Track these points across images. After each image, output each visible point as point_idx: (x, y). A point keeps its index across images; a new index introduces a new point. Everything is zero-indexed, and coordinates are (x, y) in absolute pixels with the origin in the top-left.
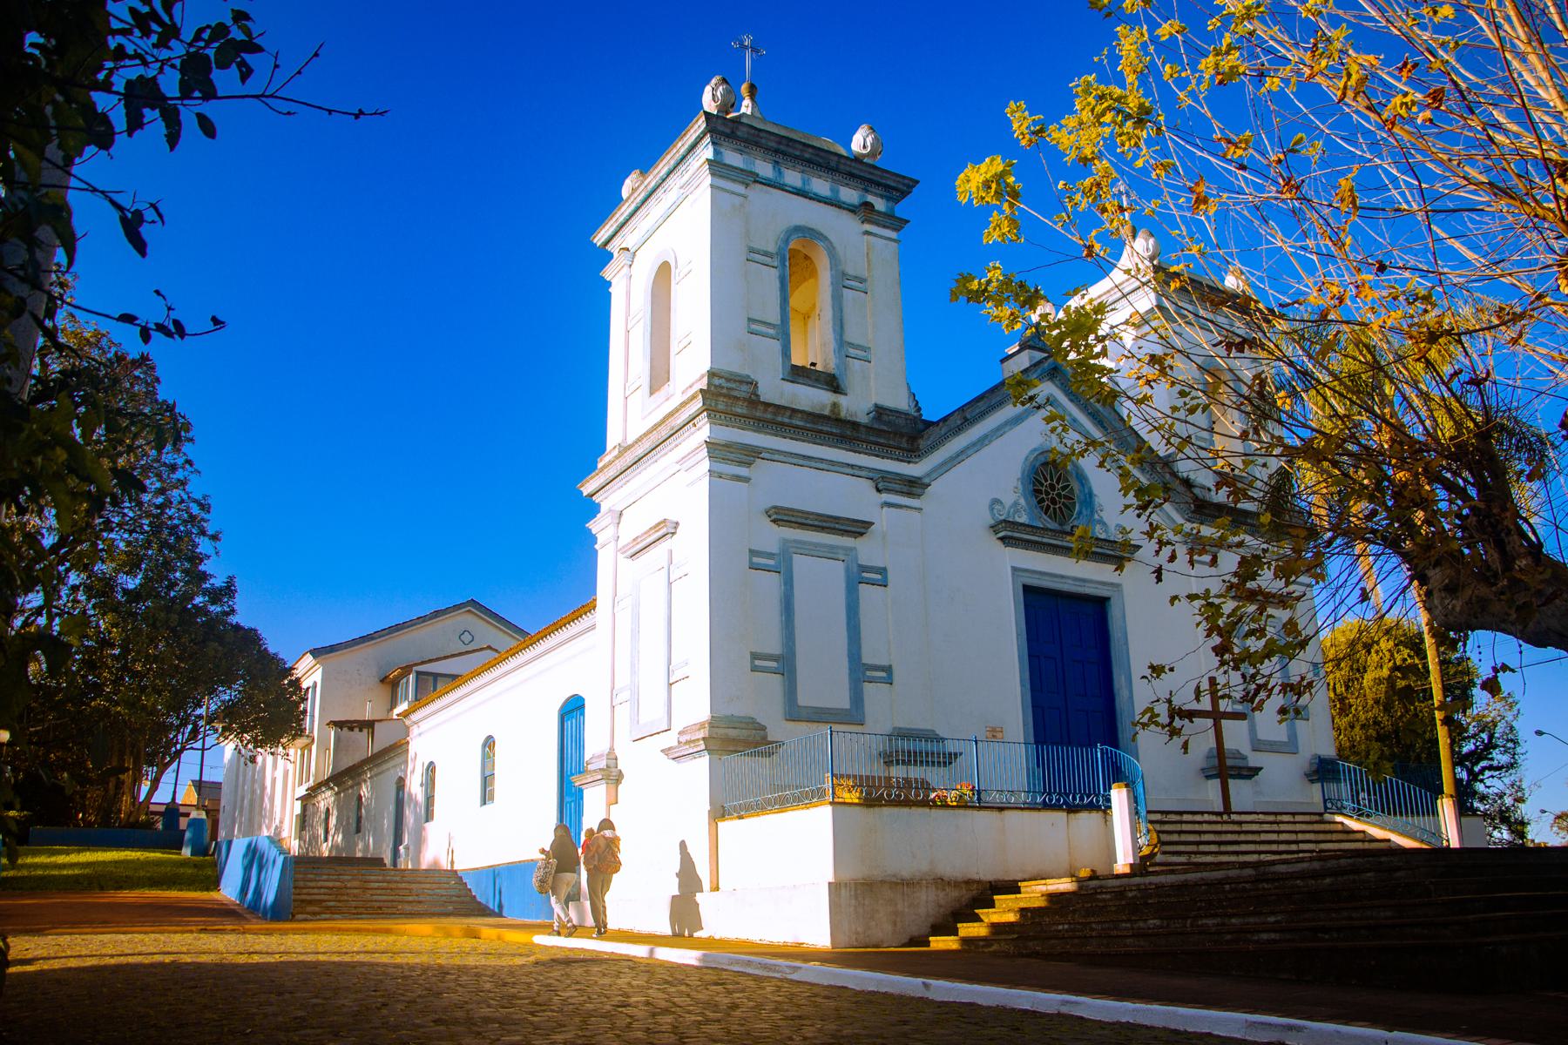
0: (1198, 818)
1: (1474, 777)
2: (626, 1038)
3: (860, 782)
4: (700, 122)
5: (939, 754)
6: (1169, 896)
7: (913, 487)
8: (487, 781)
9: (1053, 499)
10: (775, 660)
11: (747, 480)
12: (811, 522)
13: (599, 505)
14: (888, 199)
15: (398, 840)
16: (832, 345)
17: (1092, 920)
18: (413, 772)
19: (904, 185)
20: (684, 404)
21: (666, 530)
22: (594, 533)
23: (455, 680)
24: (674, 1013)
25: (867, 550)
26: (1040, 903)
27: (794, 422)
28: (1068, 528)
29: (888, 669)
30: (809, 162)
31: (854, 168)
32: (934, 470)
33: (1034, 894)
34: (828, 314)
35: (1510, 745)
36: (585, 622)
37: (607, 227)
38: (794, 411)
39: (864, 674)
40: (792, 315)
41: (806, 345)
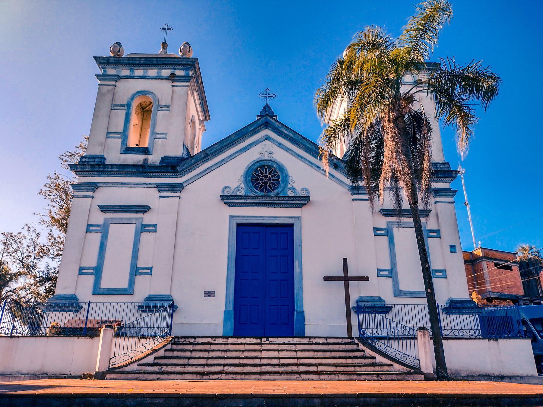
10: (92, 269)
12: (118, 210)
25: (148, 218)
27: (113, 170)
31: (165, 61)
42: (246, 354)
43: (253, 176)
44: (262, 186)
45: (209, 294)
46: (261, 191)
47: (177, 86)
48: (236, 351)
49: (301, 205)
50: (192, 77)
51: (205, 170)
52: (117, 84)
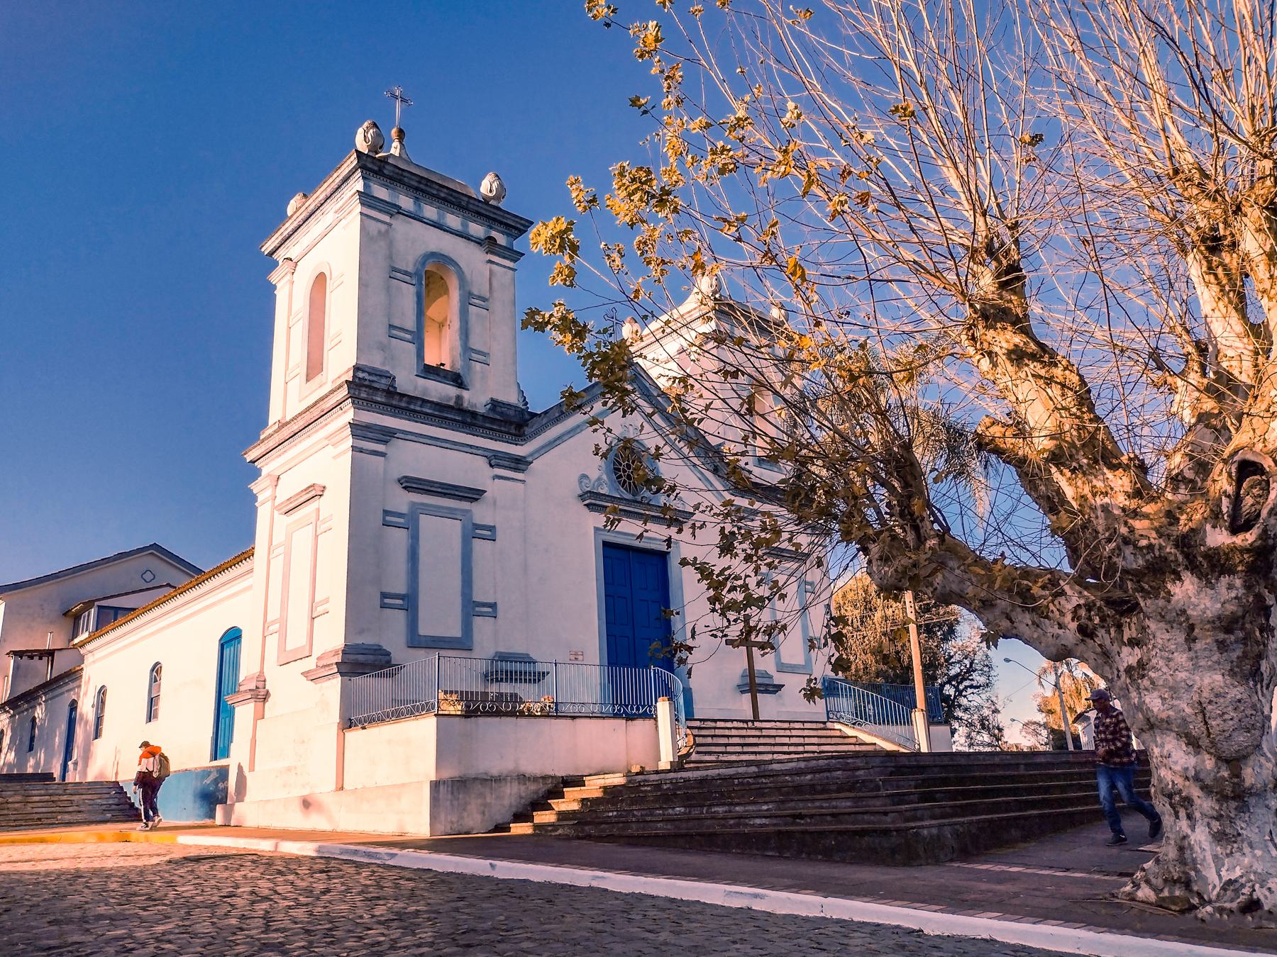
0: (729, 725)
1: (960, 693)
2: (219, 925)
3: (465, 697)
4: (352, 158)
5: (525, 673)
6: (694, 788)
7: (519, 464)
8: (152, 702)
9: (629, 475)
11: (383, 454)
13: (260, 470)
14: (508, 235)
15: (68, 754)
16: (459, 349)
17: (634, 807)
18: (85, 694)
19: (522, 224)
20: (332, 392)
21: (315, 492)
22: (255, 492)
23: (128, 613)
24: (271, 900)
25: (480, 513)
26: (599, 794)
28: (639, 498)
29: (493, 606)
30: (444, 200)
32: (537, 451)
33: (593, 788)
34: (456, 324)
35: (986, 669)
36: (245, 566)
37: (273, 239)
38: (424, 401)
39: (474, 609)
40: (427, 323)
41: (440, 348)
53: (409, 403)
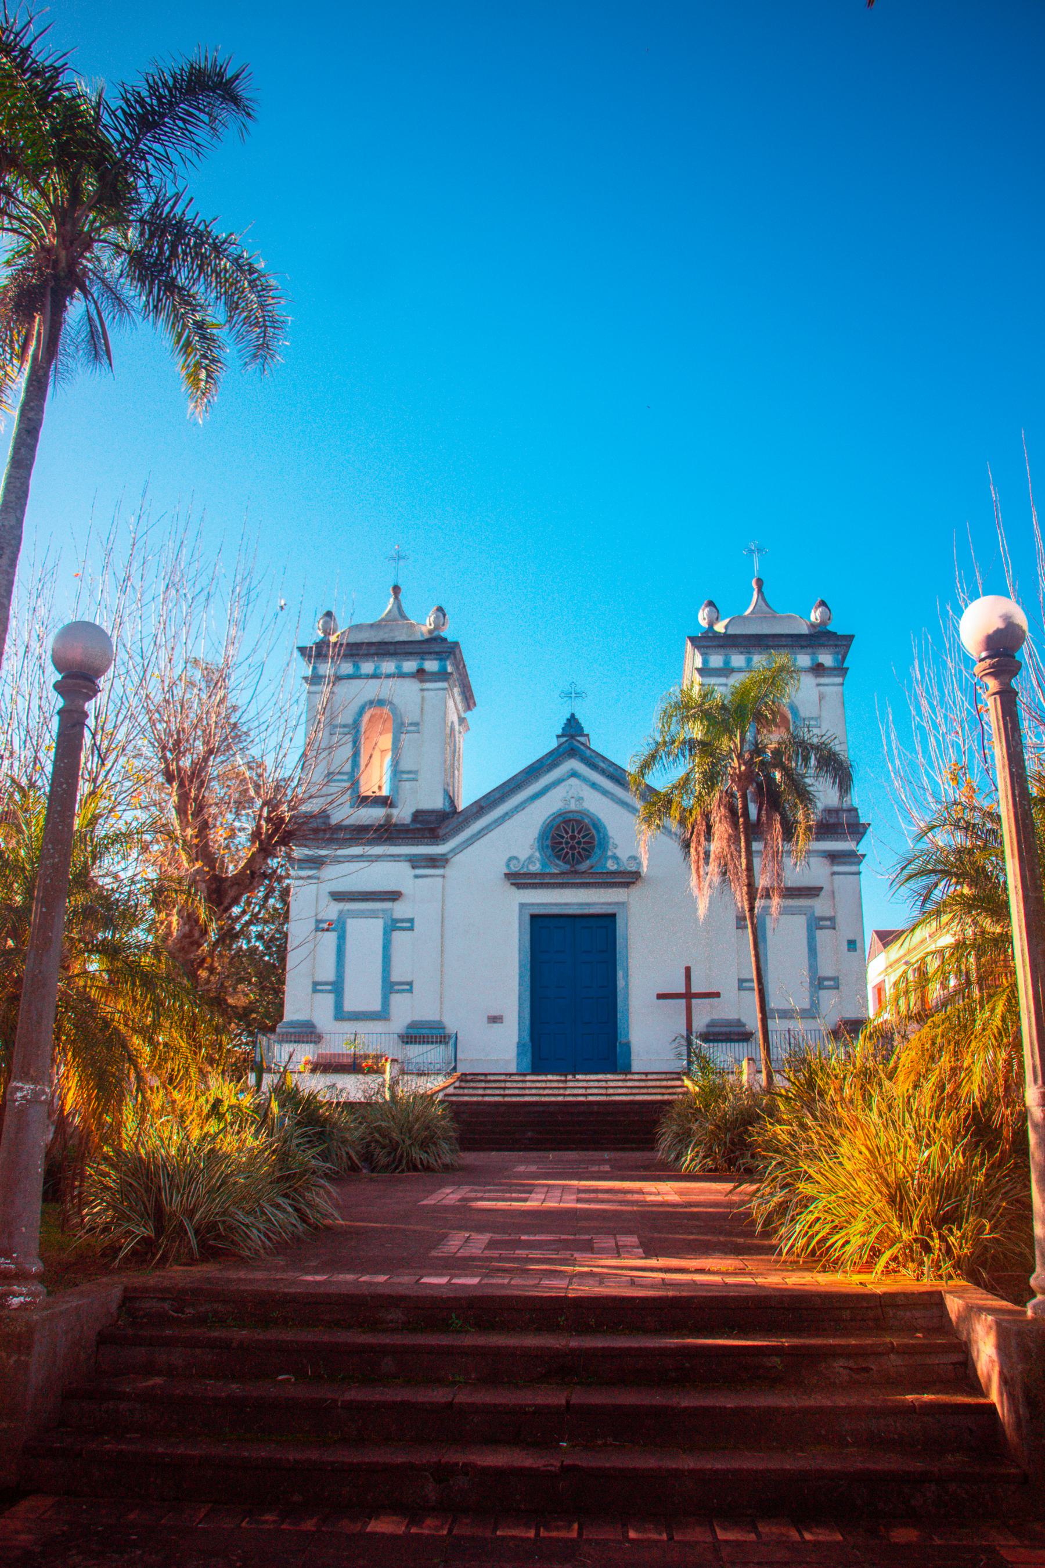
25: (400, 910)
42: (547, 1092)
43: (553, 838)
44: (567, 853)
45: (495, 1019)
46: (565, 863)
47: (428, 690)
48: (536, 1088)
49: (627, 885)
50: (451, 674)
51: (479, 832)
52: (335, 689)
53: (332, 834)
